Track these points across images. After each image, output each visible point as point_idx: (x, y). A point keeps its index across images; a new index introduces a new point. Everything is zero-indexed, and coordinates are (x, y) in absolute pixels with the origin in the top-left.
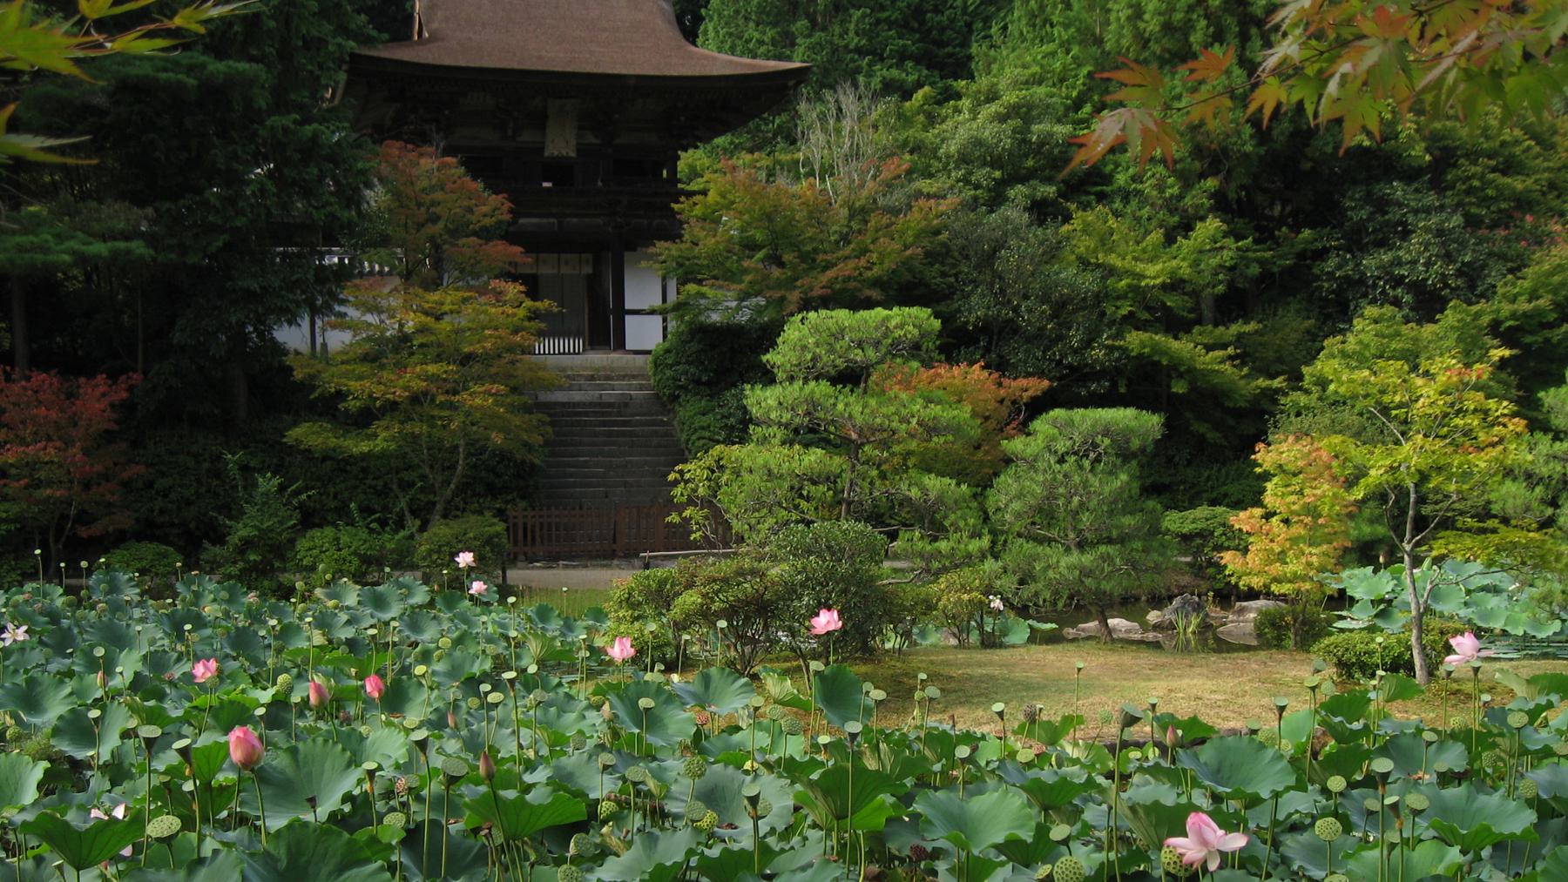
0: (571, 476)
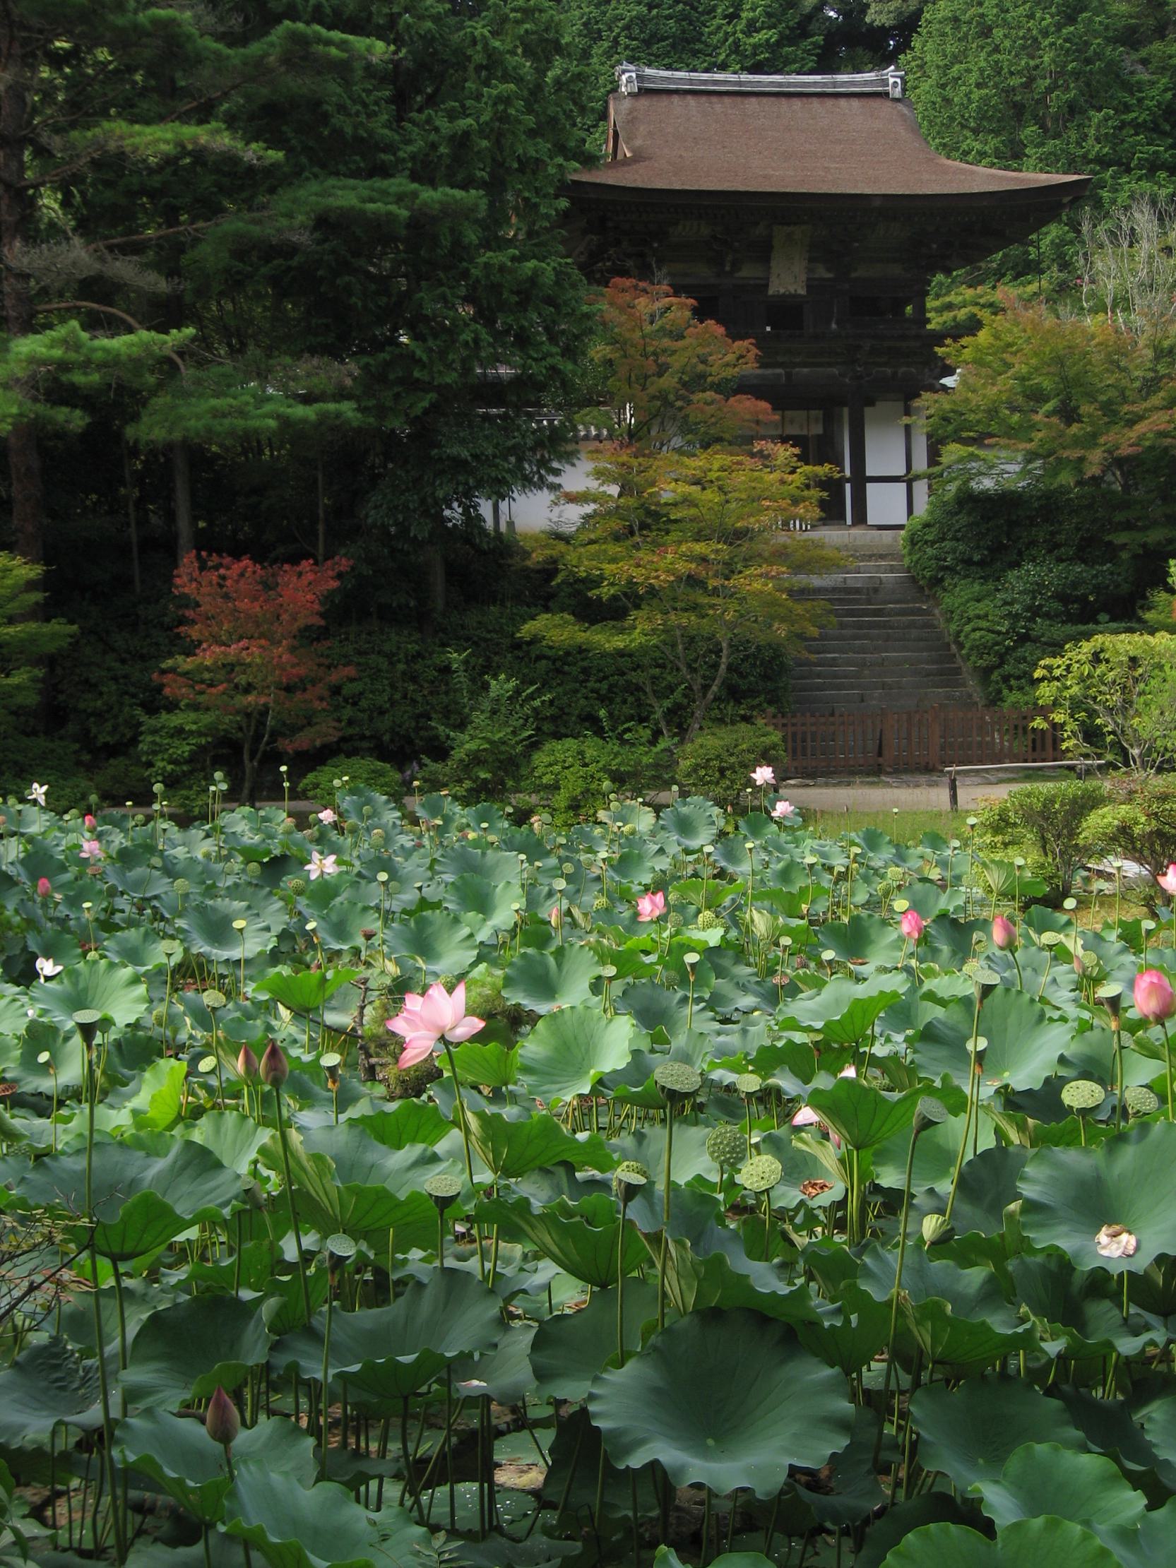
0: (819, 676)
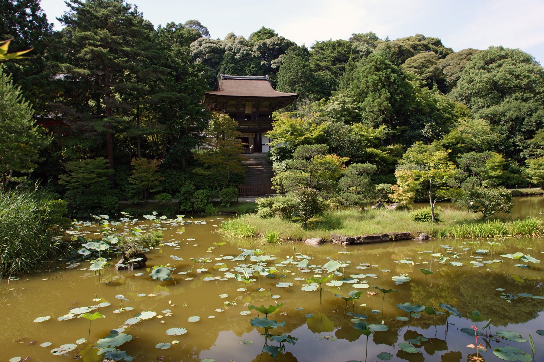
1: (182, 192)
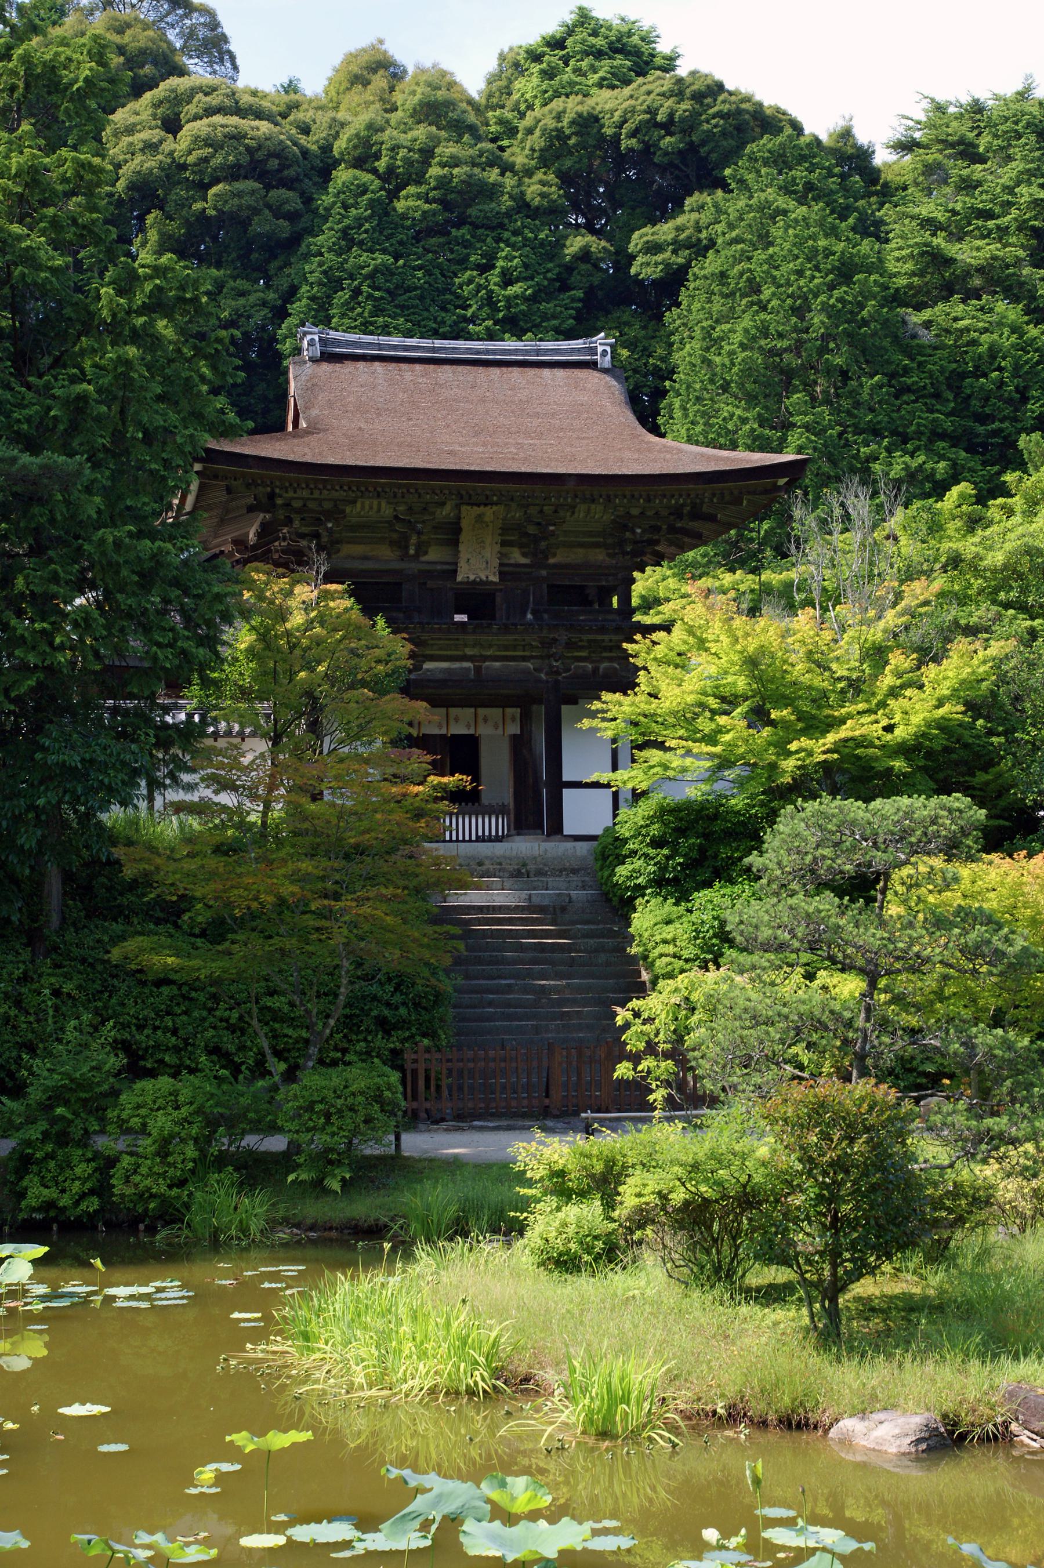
0: (490, 1004)
1: (35, 1094)
